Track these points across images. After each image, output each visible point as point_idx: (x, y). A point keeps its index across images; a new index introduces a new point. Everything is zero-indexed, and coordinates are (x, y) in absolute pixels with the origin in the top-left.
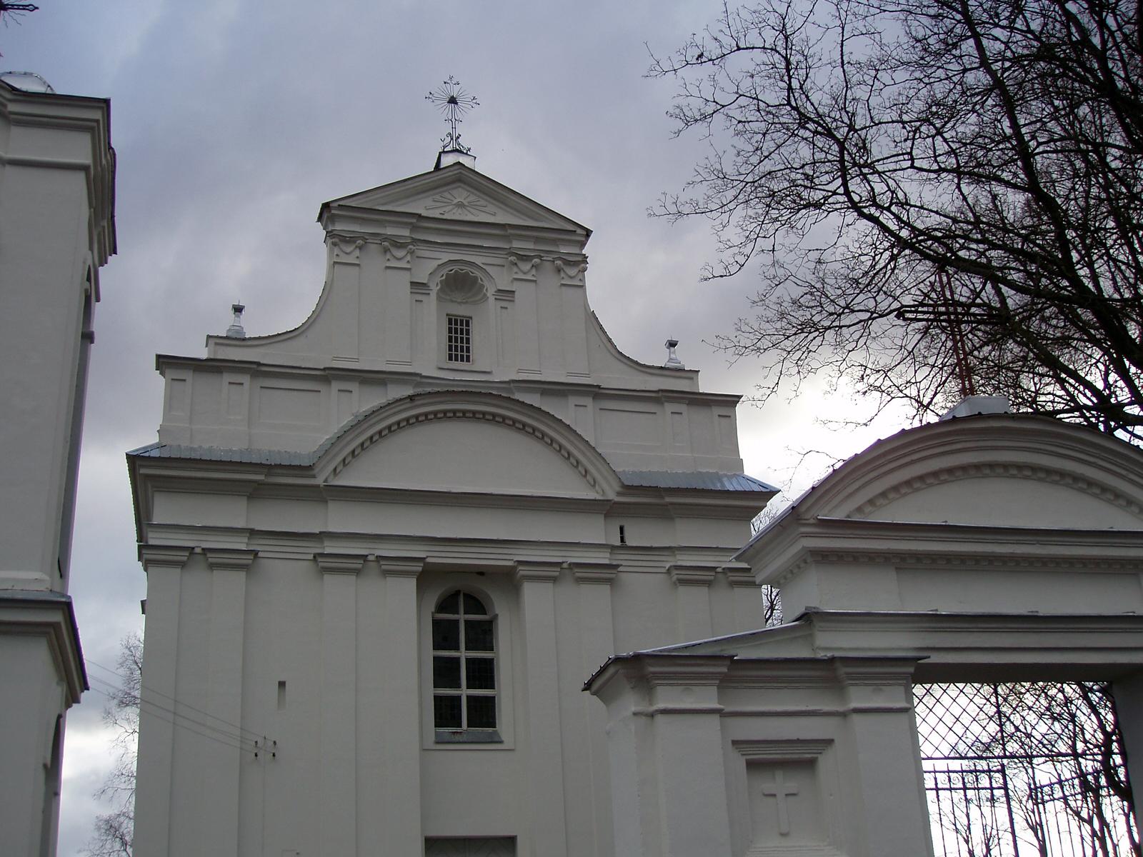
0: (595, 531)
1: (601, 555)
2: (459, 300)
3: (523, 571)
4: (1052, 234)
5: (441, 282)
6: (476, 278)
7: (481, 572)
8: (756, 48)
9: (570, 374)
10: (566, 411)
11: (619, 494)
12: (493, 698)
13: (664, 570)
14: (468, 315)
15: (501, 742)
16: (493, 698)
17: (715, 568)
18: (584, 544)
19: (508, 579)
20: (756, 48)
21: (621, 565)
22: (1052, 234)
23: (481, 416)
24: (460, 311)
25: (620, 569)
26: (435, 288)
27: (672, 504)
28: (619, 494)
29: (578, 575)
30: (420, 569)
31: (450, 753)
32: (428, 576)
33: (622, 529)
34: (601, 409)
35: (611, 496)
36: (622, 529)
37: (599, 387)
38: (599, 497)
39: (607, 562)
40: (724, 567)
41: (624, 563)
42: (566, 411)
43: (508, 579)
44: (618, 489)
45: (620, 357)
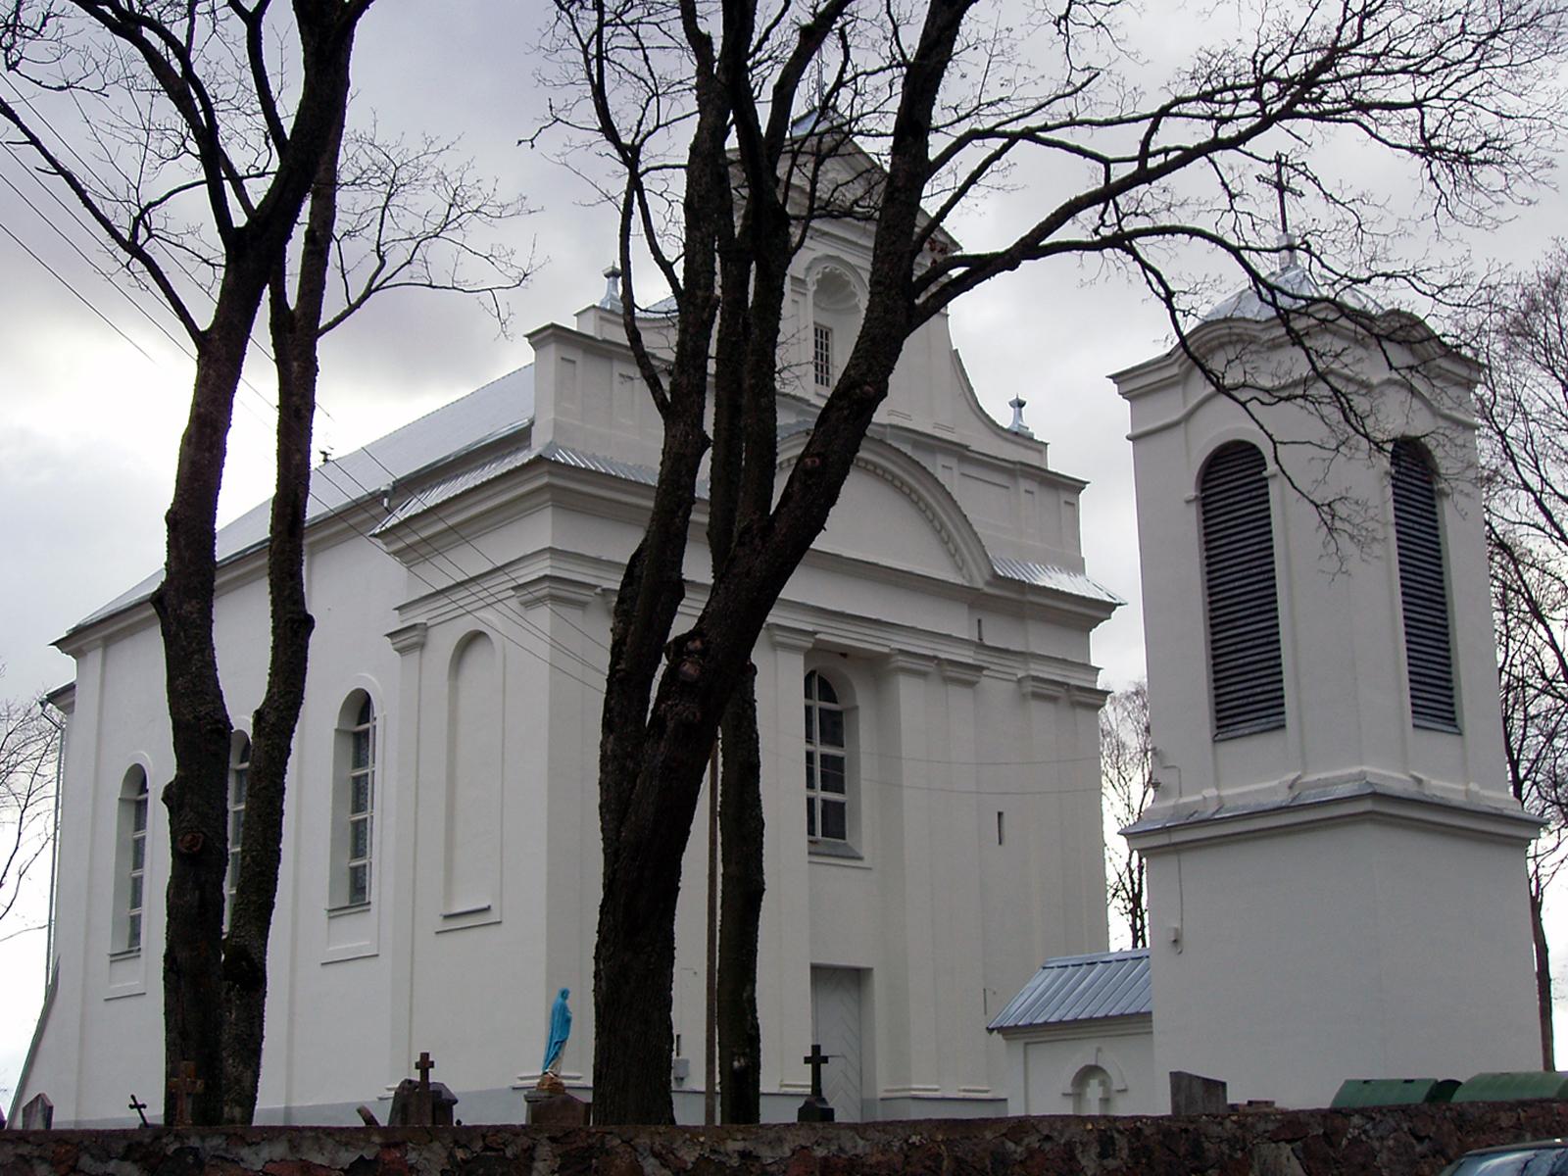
0: (956, 622)
1: (967, 653)
2: (823, 305)
3: (901, 661)
4: (1429, 348)
5: (818, 280)
6: (848, 282)
7: (844, 653)
8: (1264, 161)
9: (937, 426)
10: (942, 468)
11: (988, 584)
12: (842, 805)
13: (1015, 678)
14: (828, 325)
15: (860, 858)
16: (842, 805)
17: (596, 587)
18: (956, 638)
19: (877, 667)
20: (1264, 161)
21: (988, 668)
22: (1429, 348)
23: (890, 478)
24: (826, 321)
25: (985, 672)
26: (812, 288)
27: (1031, 603)
28: (988, 584)
29: (948, 674)
30: (810, 645)
31: (834, 869)
32: (810, 654)
33: (979, 621)
34: (963, 475)
35: (980, 584)
36: (979, 621)
37: (966, 447)
38: (966, 584)
39: (971, 661)
40: (605, 586)
41: (993, 667)
42: (942, 468)
43: (877, 667)
44: (988, 577)
45: (977, 411)
